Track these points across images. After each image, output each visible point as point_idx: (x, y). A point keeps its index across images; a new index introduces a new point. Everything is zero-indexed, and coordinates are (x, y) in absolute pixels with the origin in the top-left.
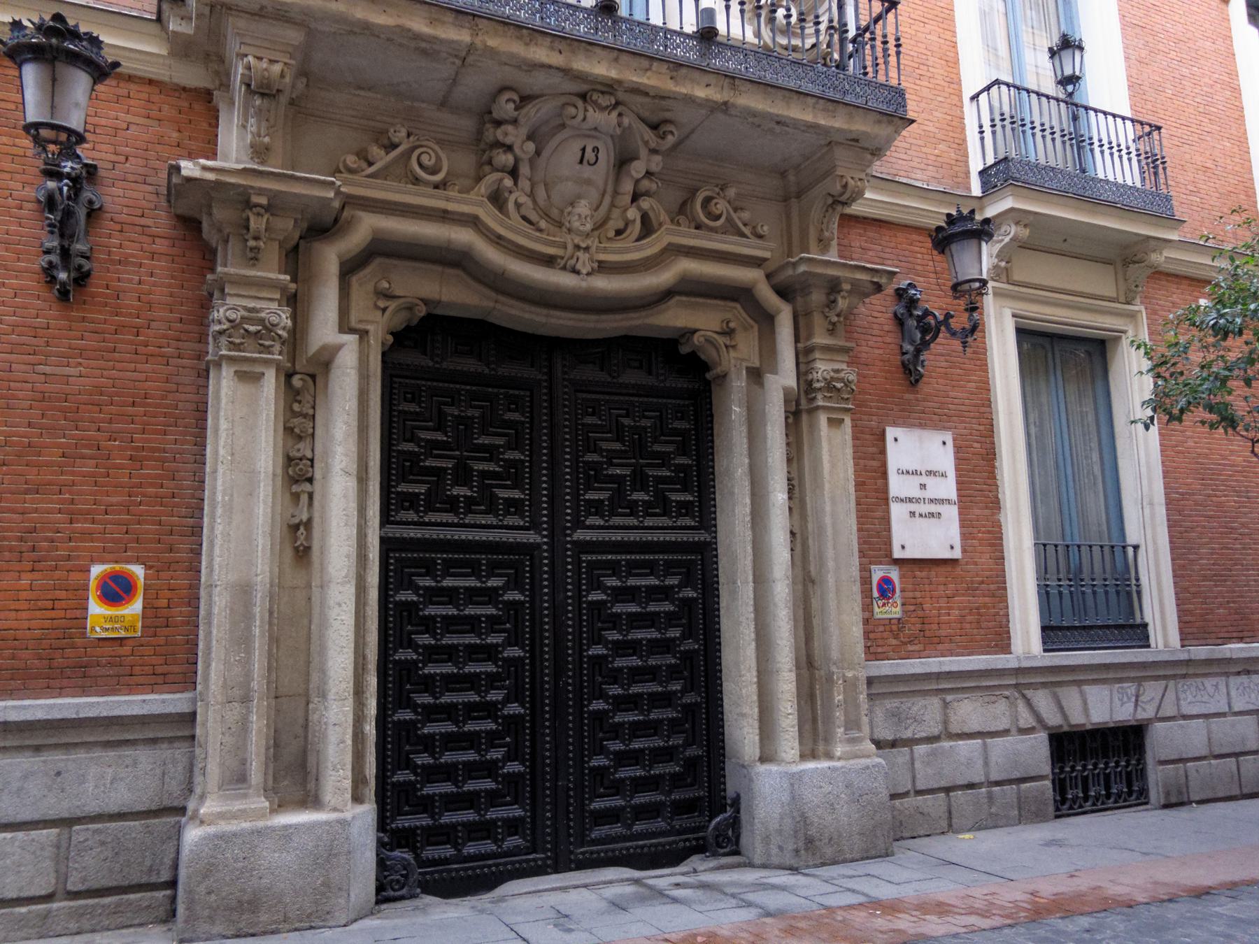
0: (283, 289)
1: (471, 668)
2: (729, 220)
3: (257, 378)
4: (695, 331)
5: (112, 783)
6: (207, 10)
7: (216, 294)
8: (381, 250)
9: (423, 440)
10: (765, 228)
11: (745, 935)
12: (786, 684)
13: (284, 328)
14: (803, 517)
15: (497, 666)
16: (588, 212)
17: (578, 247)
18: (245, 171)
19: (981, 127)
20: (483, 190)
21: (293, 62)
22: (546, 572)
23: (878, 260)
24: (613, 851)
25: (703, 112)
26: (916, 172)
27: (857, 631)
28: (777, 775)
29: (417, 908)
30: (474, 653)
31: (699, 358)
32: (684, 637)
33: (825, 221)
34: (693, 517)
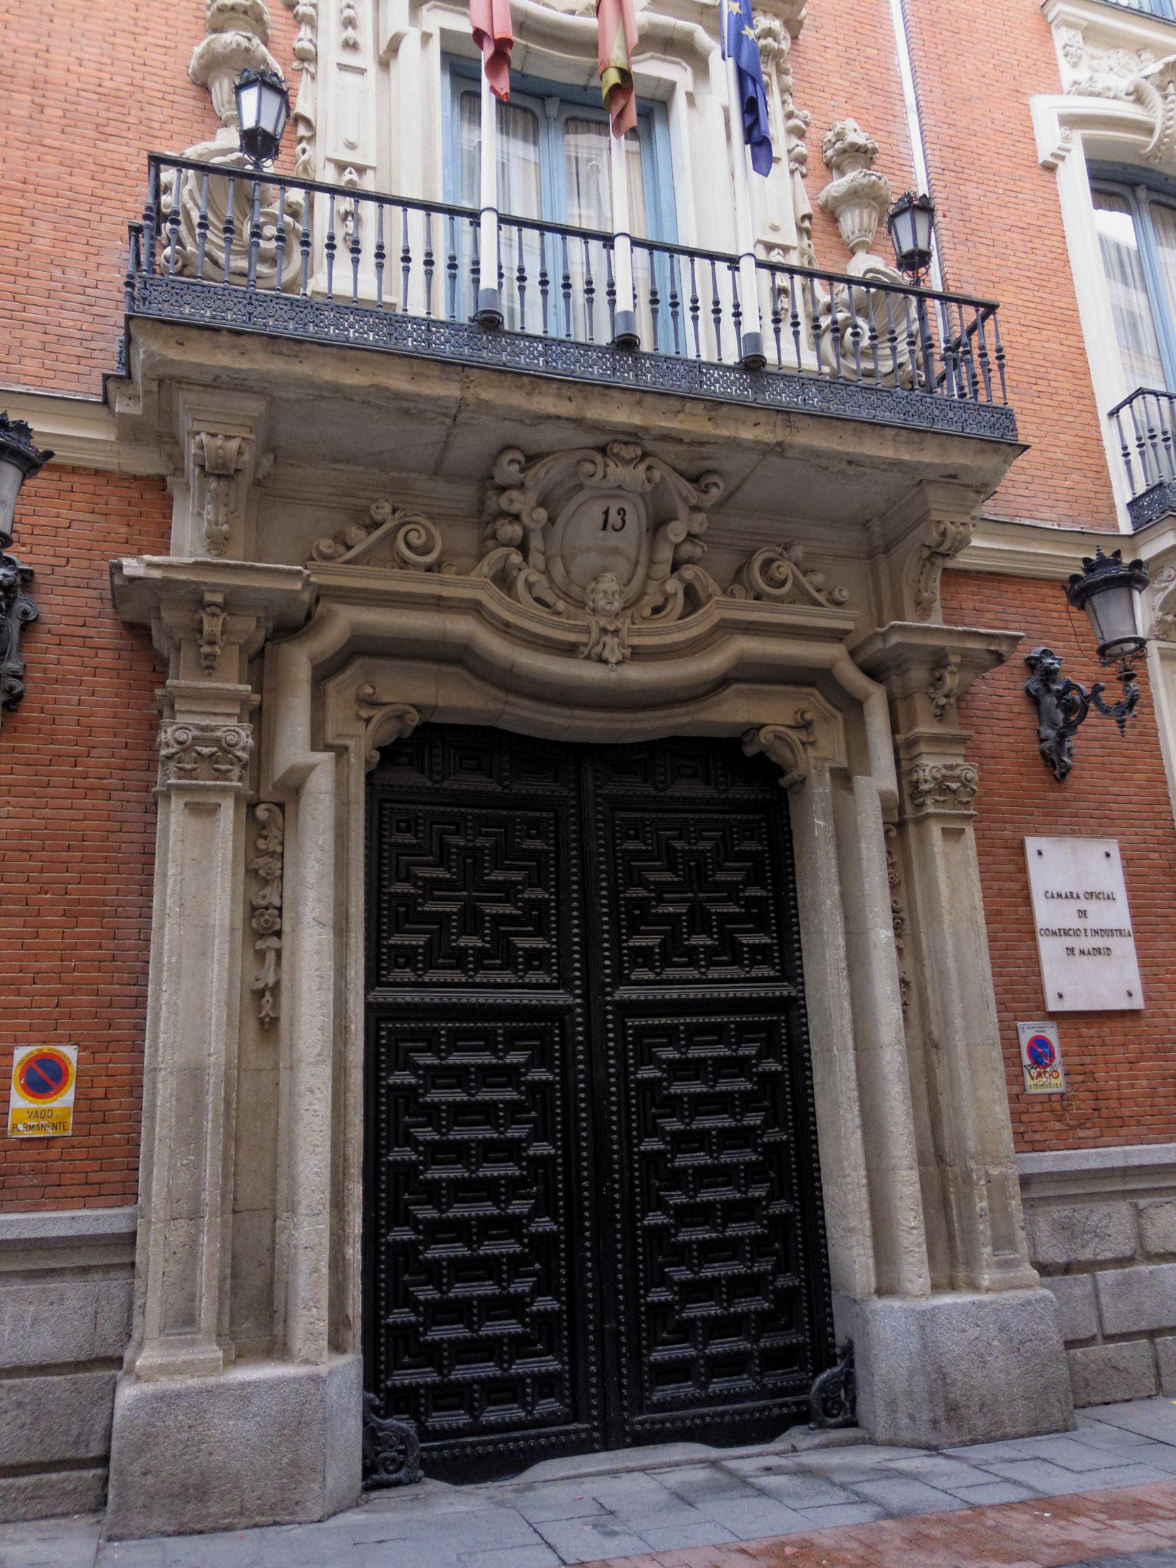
0: (243, 702)
1: (487, 1171)
2: (797, 585)
3: (211, 810)
4: (761, 726)
5: (32, 1325)
6: (154, 386)
7: (166, 712)
8: (362, 649)
9: (421, 878)
10: (845, 593)
11: (854, 1545)
12: (906, 1186)
13: (244, 749)
14: (918, 959)
15: (521, 1168)
16: (617, 588)
17: (604, 631)
18: (197, 565)
19: (1125, 448)
20: (485, 569)
21: (252, 436)
22: (580, 1043)
23: (997, 623)
24: (683, 1419)
25: (754, 456)
26: (1033, 513)
27: (1002, 1112)
28: (903, 1313)
29: (416, 1498)
30: (490, 1150)
31: (768, 759)
32: (767, 1125)
33: (923, 578)
34: (772, 965)
